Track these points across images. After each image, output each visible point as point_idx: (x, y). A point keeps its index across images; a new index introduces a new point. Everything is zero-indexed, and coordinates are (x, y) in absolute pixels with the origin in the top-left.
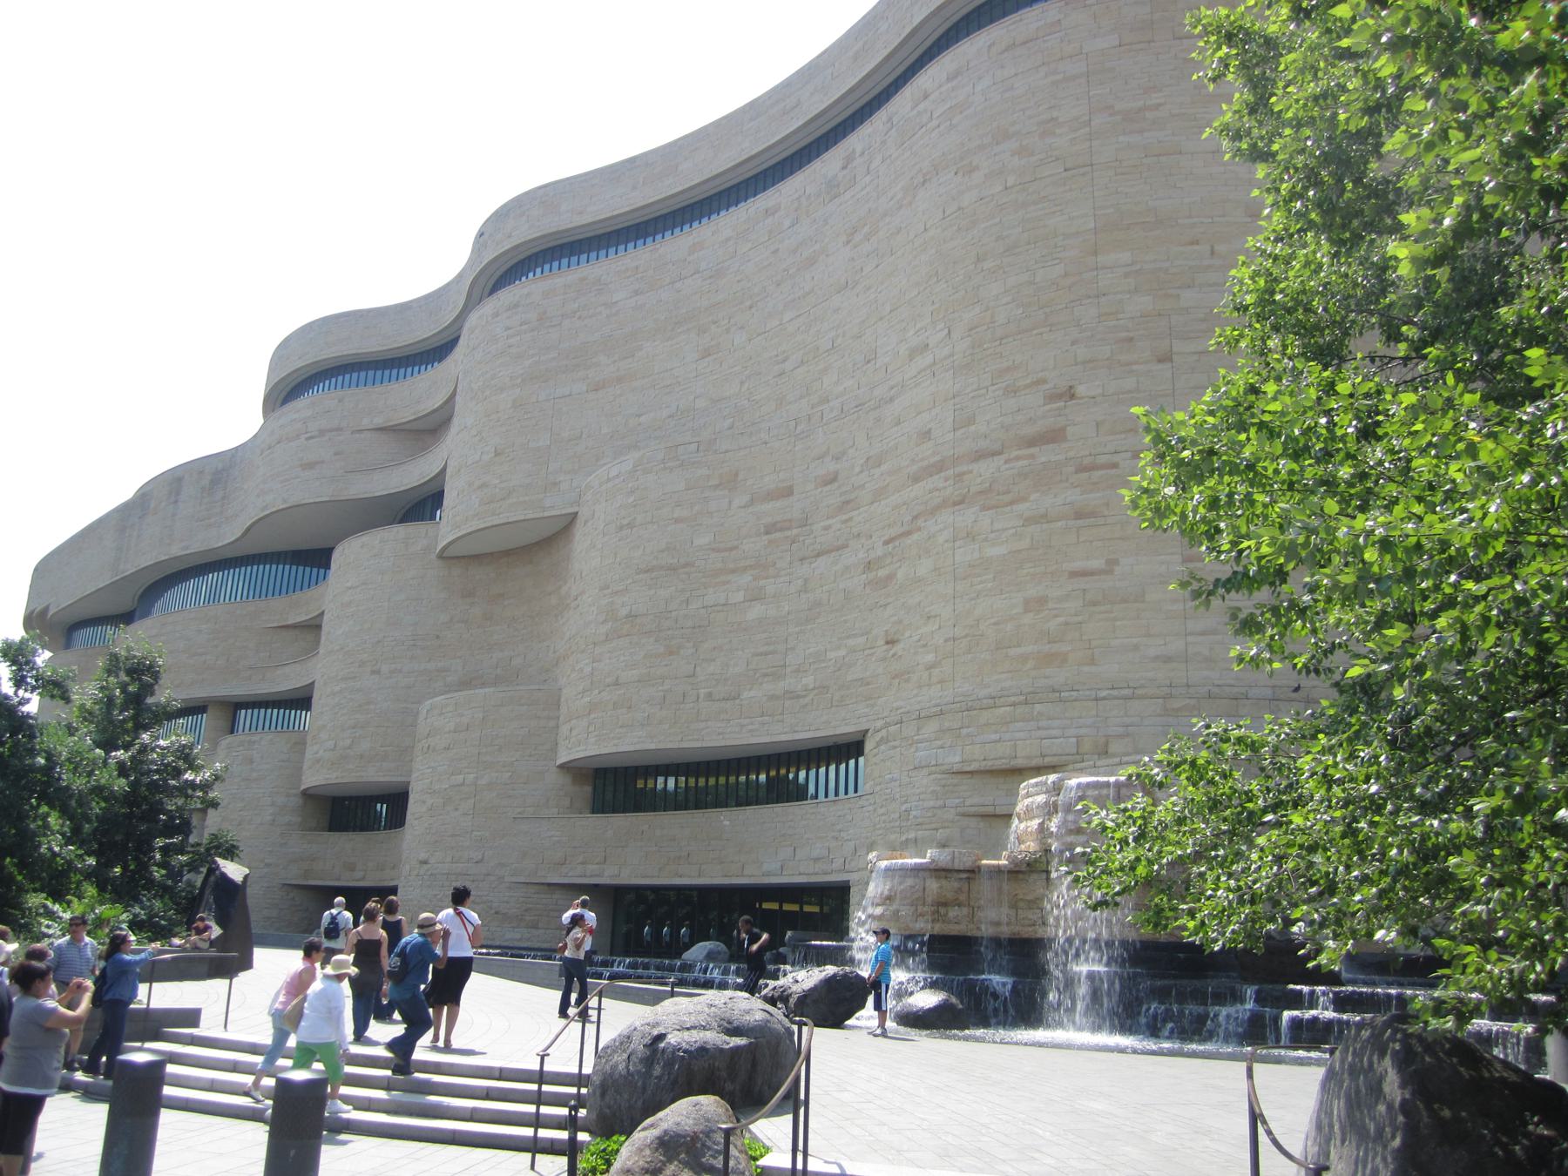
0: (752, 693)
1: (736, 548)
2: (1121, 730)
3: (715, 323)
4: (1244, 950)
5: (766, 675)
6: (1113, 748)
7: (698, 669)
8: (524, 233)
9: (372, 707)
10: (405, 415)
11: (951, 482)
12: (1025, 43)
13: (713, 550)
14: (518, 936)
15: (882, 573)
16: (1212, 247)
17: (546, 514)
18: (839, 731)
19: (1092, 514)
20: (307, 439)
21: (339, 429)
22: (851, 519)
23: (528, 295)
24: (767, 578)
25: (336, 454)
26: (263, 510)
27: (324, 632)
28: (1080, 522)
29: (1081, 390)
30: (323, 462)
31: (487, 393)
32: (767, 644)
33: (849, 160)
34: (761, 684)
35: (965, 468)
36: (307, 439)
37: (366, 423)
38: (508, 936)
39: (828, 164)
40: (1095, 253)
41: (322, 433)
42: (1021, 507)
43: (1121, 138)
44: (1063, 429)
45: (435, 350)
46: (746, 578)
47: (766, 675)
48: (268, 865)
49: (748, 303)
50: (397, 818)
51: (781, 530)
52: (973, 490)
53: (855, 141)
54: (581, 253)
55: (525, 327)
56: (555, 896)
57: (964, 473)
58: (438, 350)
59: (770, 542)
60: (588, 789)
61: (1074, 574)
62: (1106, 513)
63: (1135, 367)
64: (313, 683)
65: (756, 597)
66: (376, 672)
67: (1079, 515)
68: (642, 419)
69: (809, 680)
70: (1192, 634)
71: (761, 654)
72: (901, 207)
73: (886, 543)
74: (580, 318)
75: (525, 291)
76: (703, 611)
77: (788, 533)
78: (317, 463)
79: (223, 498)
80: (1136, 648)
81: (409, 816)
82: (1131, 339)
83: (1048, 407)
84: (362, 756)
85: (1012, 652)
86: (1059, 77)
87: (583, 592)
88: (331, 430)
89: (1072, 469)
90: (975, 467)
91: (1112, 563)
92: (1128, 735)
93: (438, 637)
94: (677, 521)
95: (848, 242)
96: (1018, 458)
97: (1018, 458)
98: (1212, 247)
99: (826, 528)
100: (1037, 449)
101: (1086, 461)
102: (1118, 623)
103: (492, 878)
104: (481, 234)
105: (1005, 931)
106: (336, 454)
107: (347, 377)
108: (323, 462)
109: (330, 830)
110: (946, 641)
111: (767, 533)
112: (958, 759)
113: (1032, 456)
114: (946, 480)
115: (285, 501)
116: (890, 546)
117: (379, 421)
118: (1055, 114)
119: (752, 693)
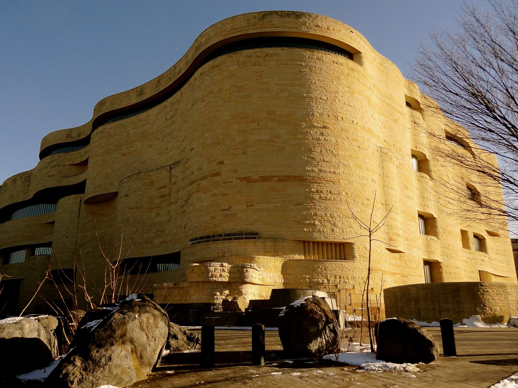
0: (156, 242)
3: (152, 138)
4: (67, 378)
6: (226, 255)
8: (105, 110)
10: (78, 161)
20: (50, 168)
21: (59, 165)
24: (160, 210)
27: (55, 224)
29: (225, 162)
33: (182, 94)
36: (50, 168)
40: (230, 125)
41: (54, 166)
42: (211, 193)
49: (160, 133)
50: (190, 240)
58: (85, 142)
61: (221, 210)
65: (158, 215)
66: (67, 237)
68: (135, 165)
69: (169, 238)
77: (165, 198)
79: (28, 185)
82: (237, 149)
83: (218, 166)
86: (224, 76)
88: (57, 166)
91: (230, 207)
93: (85, 227)
94: (140, 195)
101: (225, 181)
107: (67, 148)
112: (193, 259)
113: (213, 179)
117: (71, 162)
119: (156, 242)
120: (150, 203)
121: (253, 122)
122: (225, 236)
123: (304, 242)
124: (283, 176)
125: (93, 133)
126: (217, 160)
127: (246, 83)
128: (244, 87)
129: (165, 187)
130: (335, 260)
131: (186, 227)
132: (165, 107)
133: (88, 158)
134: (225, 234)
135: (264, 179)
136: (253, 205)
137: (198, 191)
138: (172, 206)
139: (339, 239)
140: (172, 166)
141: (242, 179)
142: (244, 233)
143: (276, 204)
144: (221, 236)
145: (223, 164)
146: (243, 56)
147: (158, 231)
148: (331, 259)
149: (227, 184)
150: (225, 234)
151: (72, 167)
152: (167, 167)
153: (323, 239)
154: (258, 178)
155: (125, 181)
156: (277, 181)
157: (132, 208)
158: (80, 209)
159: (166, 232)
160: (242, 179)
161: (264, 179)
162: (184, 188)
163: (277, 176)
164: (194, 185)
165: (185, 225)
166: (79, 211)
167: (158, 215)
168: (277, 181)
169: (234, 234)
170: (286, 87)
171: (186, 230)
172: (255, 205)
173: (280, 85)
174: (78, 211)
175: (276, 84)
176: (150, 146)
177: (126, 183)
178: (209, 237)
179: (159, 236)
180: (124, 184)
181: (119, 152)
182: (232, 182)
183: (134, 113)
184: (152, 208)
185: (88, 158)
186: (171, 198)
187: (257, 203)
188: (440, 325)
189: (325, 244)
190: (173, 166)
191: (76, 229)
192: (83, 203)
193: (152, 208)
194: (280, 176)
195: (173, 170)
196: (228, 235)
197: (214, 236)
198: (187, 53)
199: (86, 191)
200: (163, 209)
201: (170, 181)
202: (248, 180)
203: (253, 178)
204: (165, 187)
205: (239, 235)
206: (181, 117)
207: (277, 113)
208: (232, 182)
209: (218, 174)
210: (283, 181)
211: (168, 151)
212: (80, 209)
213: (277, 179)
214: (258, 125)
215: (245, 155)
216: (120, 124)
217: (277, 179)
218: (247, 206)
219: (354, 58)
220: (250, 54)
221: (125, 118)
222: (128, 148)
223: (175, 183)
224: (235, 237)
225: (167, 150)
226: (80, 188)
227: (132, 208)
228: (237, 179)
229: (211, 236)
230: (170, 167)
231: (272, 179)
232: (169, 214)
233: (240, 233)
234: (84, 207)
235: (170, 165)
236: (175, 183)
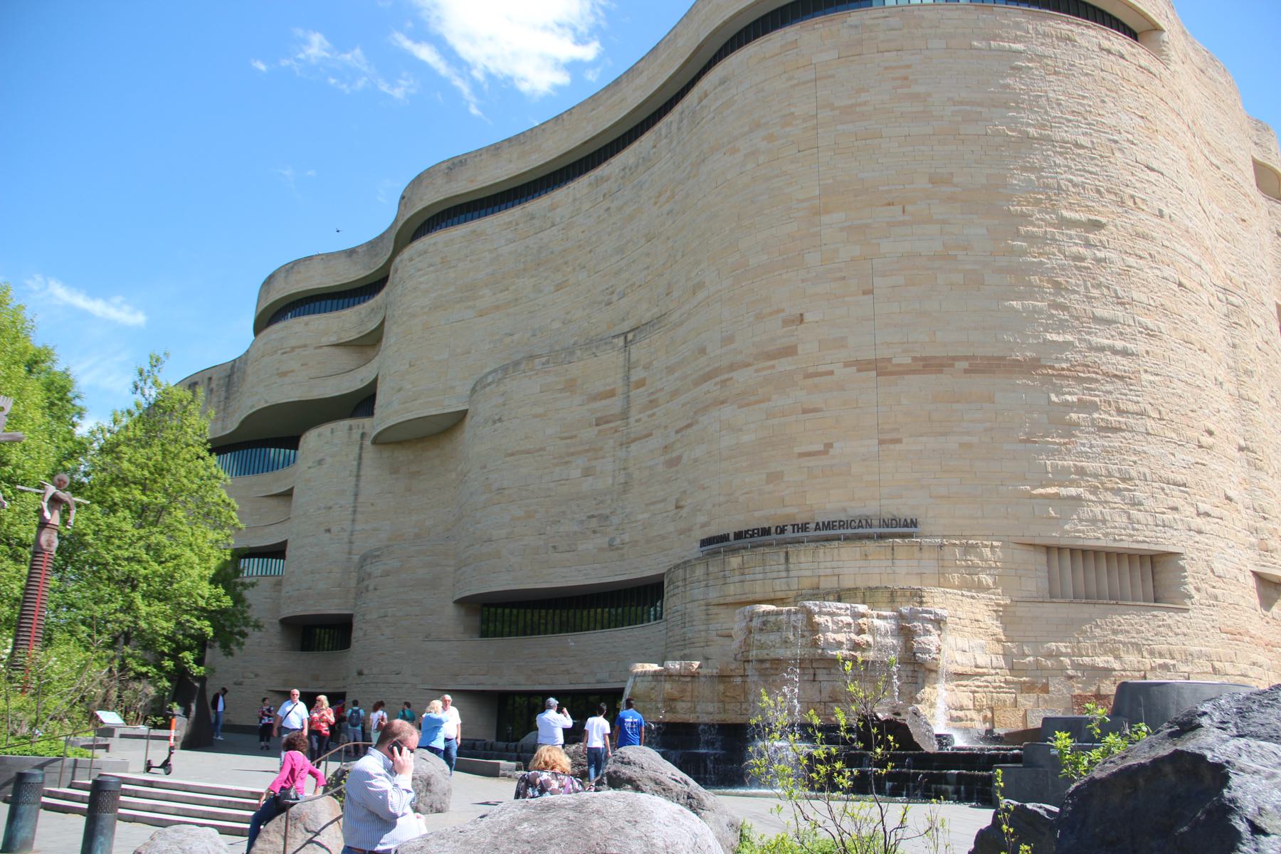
11: (719, 387)
12: (772, 57)
15: (674, 455)
16: (904, 207)
18: (645, 574)
22: (653, 415)
24: (597, 459)
25: (302, 365)
26: (251, 408)
31: (405, 319)
35: (726, 376)
37: (325, 341)
39: (647, 139)
43: (839, 127)
45: (370, 285)
49: (588, 249)
51: (607, 422)
53: (661, 126)
54: (481, 208)
55: (431, 268)
59: (600, 431)
61: (801, 455)
63: (846, 299)
64: (286, 541)
65: (587, 473)
68: (515, 337)
72: (689, 178)
73: (677, 432)
77: (612, 425)
81: (353, 640)
82: (844, 278)
83: (785, 329)
86: (795, 82)
87: (469, 471)
91: (829, 446)
95: (656, 203)
96: (764, 369)
98: (904, 207)
99: (638, 421)
100: (777, 361)
101: (811, 370)
104: (403, 197)
105: (718, 718)
113: (773, 367)
114: (716, 384)
115: (266, 402)
116: (680, 434)
117: (333, 339)
118: (792, 110)
120: (566, 438)
121: (889, 204)
122: (817, 528)
123: (1048, 549)
124: (982, 358)
125: (398, 259)
126: (783, 310)
127: (864, 97)
128: (858, 109)
129: (612, 394)
130: (1142, 603)
131: (683, 503)
132: (605, 179)
133: (382, 323)
134: (818, 524)
135: (930, 365)
136: (898, 441)
137: (723, 402)
138: (633, 447)
139: (1148, 538)
140: (630, 336)
141: (862, 366)
142: (875, 522)
143: (966, 439)
144: (804, 527)
145: (802, 321)
146: (851, 26)
147: (590, 517)
148: (1133, 600)
149: (816, 380)
150: (818, 524)
151: (337, 351)
152: (616, 340)
153: (1104, 543)
154: (910, 361)
155: (490, 379)
156: (966, 371)
157: (512, 454)
158: (360, 457)
159: (615, 520)
160: (862, 366)
161: (930, 365)
162: (675, 393)
163: (966, 358)
164: (709, 385)
165: (677, 500)
166: (359, 465)
167: (587, 473)
168: (966, 371)
169: (842, 524)
170: (979, 109)
171: (684, 512)
172: (904, 441)
173: (961, 103)
174: (355, 463)
175: (949, 99)
176: (559, 287)
177: (493, 386)
178: (766, 532)
179: (594, 532)
180: (488, 389)
181: (470, 304)
182: (831, 373)
183: (357, 299)
184: (572, 454)
185: (382, 323)
186: (628, 424)
187: (911, 436)
188: (1031, 726)
189: (1068, 553)
190: (634, 336)
191: (351, 509)
192: (368, 442)
193: (572, 454)
194: (974, 357)
195: (633, 348)
196: (828, 525)
197: (782, 530)
198: (666, 39)
199: (375, 411)
200: (603, 457)
201: (627, 378)
202: (881, 368)
203: (895, 361)
204: (612, 394)
205: (906, 526)
206: (656, 203)
207: (955, 180)
208: (831, 373)
209: (790, 351)
210: (983, 372)
211: (615, 297)
212: (360, 457)
213: (965, 365)
214: (904, 211)
215: (866, 297)
216: (474, 231)
217: (965, 365)
218: (881, 442)
219: (1139, 38)
220: (872, 22)
221: (337, 310)
222: (495, 294)
223: (641, 383)
224: (850, 531)
225: (612, 293)
226: (362, 403)
227: (512, 454)
228: (847, 365)
229: (773, 530)
230: (626, 338)
231: (952, 365)
232: (624, 469)
233: (821, 525)
234: (370, 452)
235: (625, 334)
236: (641, 383)
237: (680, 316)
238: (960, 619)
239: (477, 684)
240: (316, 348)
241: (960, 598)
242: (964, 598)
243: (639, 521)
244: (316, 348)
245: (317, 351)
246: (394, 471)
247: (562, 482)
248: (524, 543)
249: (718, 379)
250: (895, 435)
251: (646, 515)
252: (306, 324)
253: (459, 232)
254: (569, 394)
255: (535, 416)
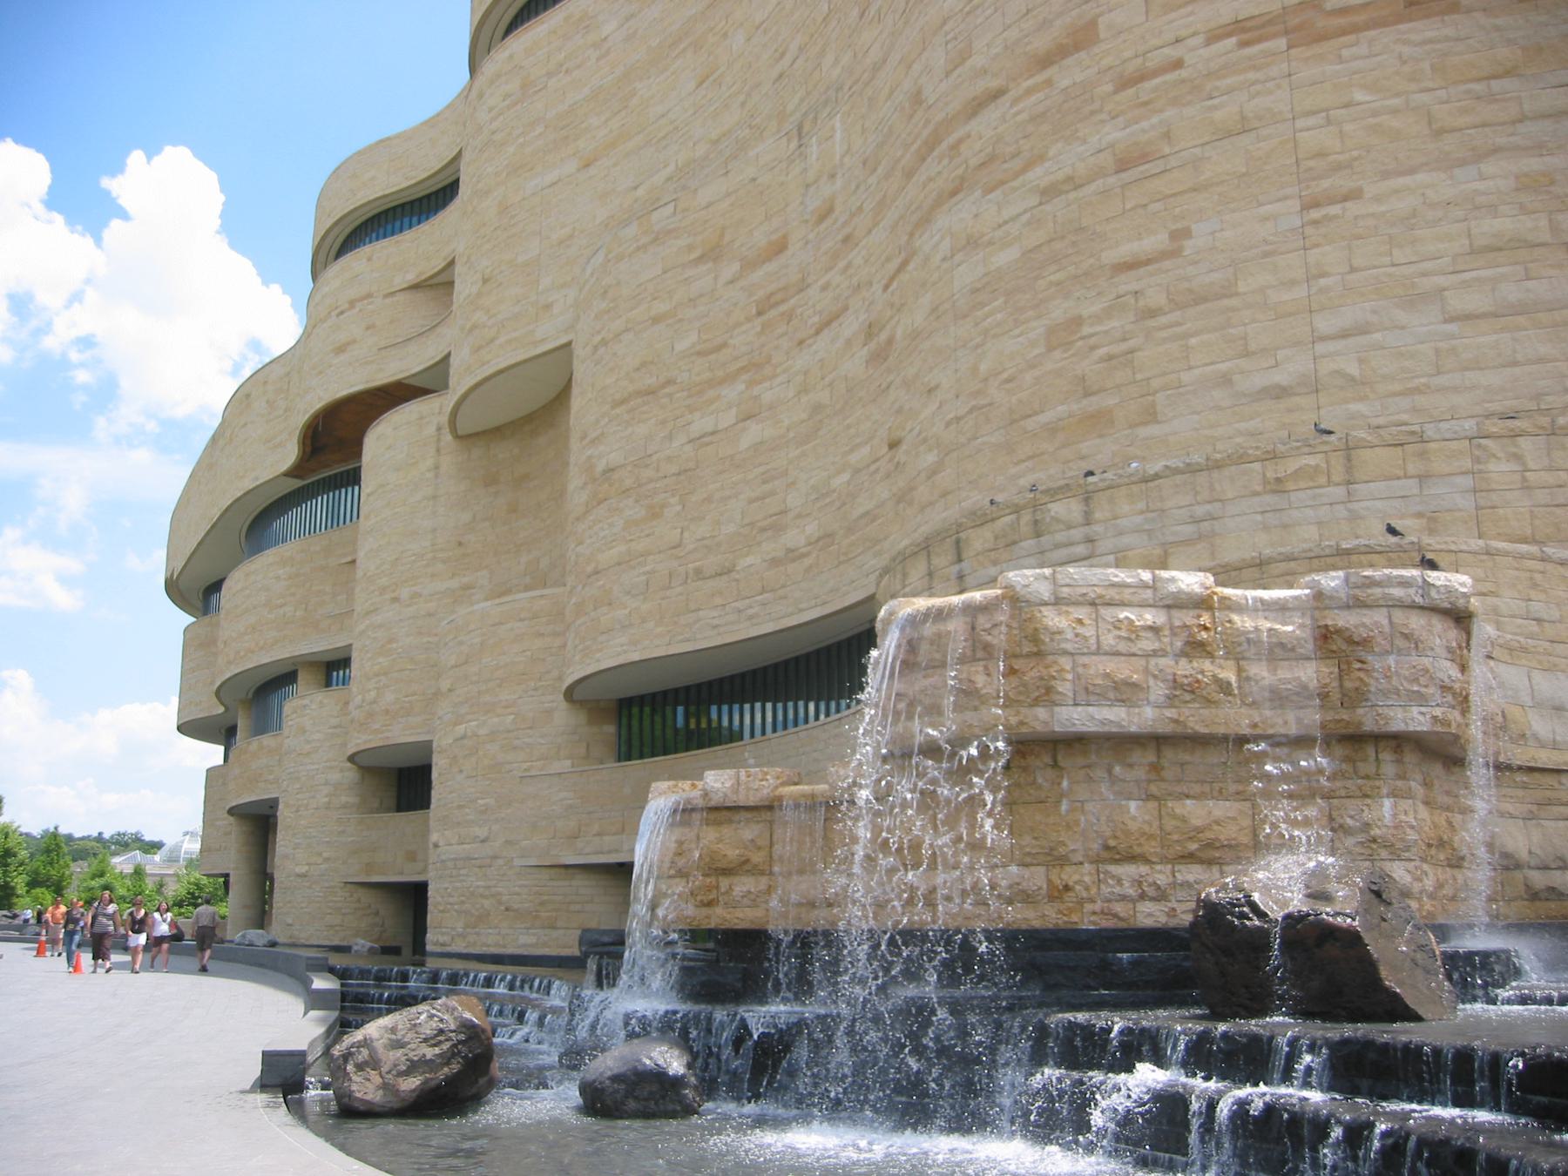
1: (724, 345)
2: (1188, 530)
5: (763, 530)
7: (686, 534)
9: (394, 645)
11: (945, 162)
13: (699, 353)
14: (533, 940)
17: (539, 350)
19: (1144, 158)
20: (338, 315)
21: (369, 296)
23: (511, 57)
25: (368, 328)
28: (1126, 176)
30: (354, 341)
32: (764, 482)
34: (759, 544)
38: (523, 939)
41: (352, 304)
44: (1092, 24)
46: (732, 392)
47: (763, 530)
48: (327, 860)
52: (974, 162)
56: (574, 883)
57: (960, 141)
60: (611, 729)
62: (1167, 150)
66: (395, 600)
67: (1122, 166)
70: (1323, 339)
71: (757, 499)
74: (567, 71)
75: (507, 54)
76: (688, 448)
78: (348, 344)
80: (1226, 380)
84: (387, 712)
85: (1030, 424)
88: (362, 299)
89: (1109, 88)
90: (975, 126)
92: (1200, 537)
96: (1029, 92)
97: (1029, 92)
101: (1131, 68)
102: (1193, 341)
103: (500, 862)
106: (368, 328)
108: (354, 341)
109: (399, 809)
110: (948, 424)
111: (760, 314)
113: (1049, 83)
117: (411, 277)
136: (1353, 195)
208: (1178, 64)
227: (623, 402)
228: (1213, 37)
237: (1461, 584)
238: (1539, 620)
239: (610, 852)
240: (386, 296)
241: (1538, 566)
242: (1549, 567)
243: (834, 491)
244: (386, 296)
245: (388, 301)
246: (490, 481)
247: (706, 440)
248: (648, 568)
249: (944, 145)
250: (1342, 182)
251: (846, 477)
252: (369, 259)
253: (545, 26)
254: (710, 265)
255: (656, 320)
